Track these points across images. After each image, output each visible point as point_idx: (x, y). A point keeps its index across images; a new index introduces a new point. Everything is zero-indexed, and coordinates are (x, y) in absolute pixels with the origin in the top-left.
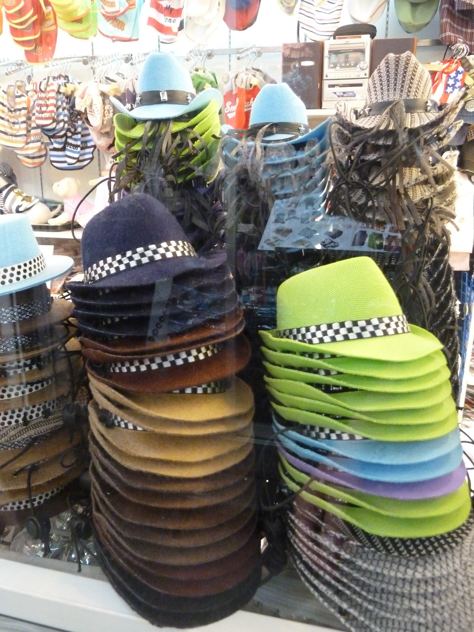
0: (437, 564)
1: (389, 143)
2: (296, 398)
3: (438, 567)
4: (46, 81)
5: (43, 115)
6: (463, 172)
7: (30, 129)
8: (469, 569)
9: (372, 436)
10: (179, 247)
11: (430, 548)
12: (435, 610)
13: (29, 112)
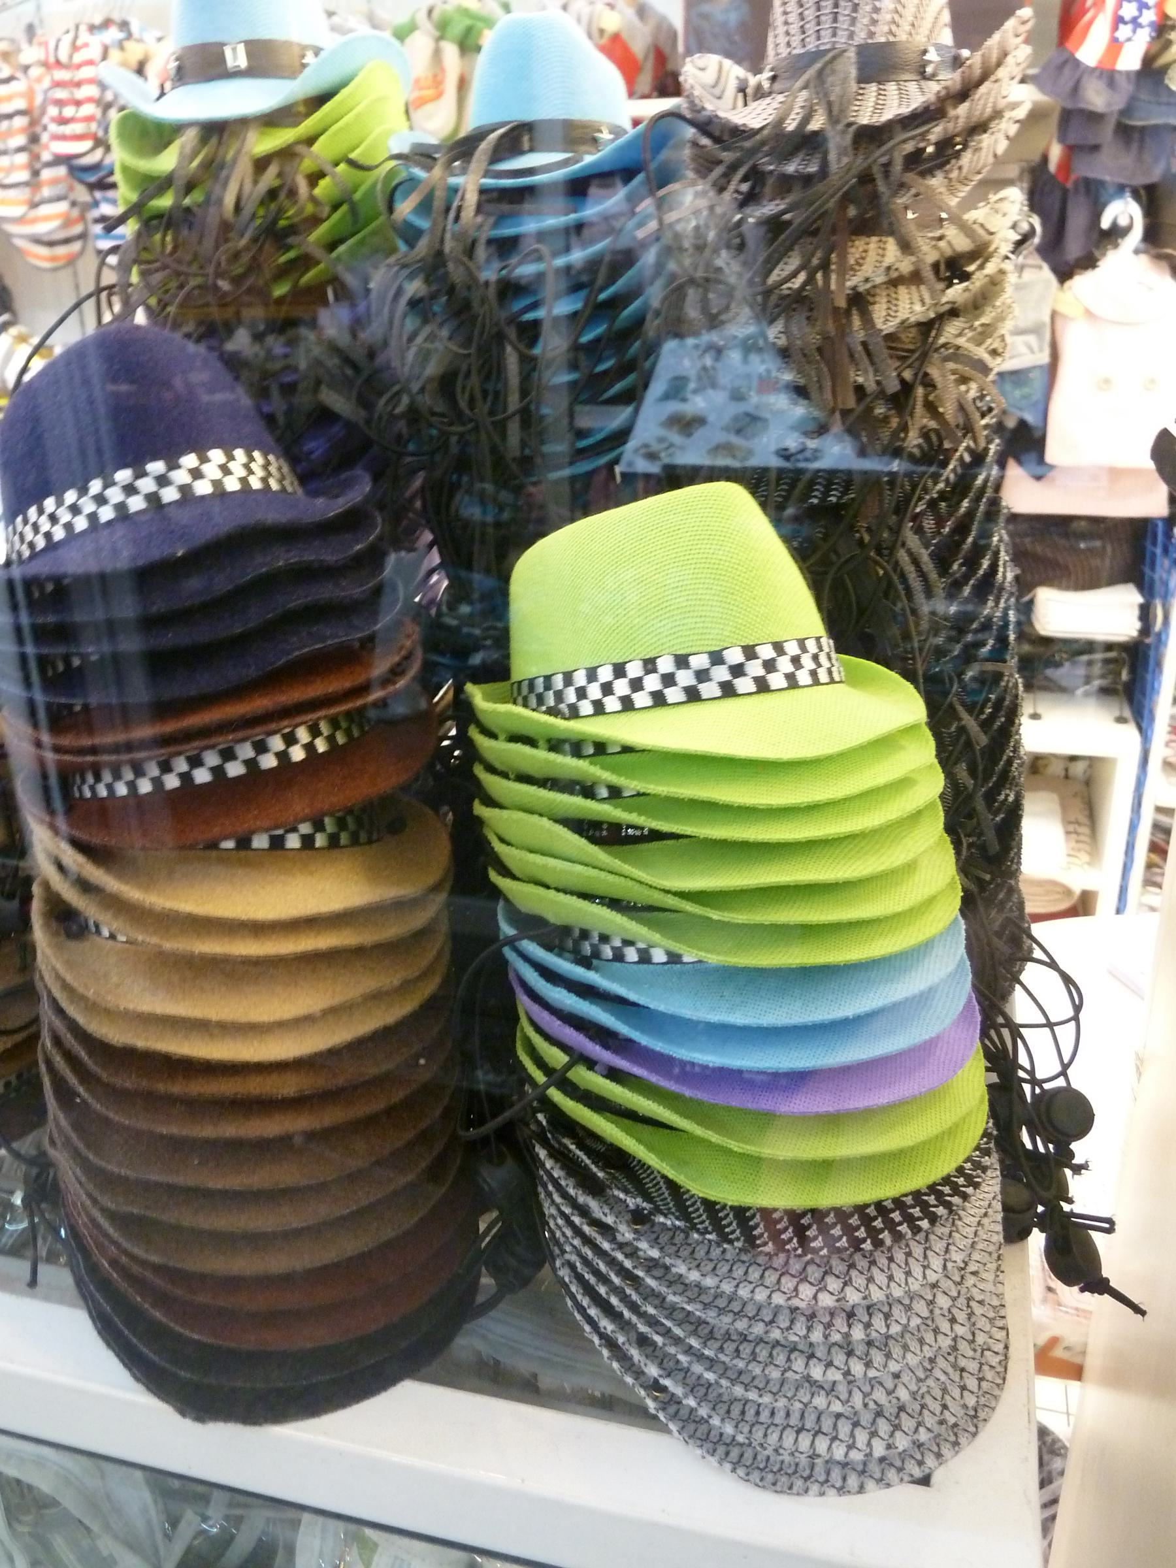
0: (882, 1271)
1: (813, 169)
2: (533, 858)
3: (880, 1278)
4: (71, 35)
5: (68, 129)
6: (1159, 257)
7: (38, 166)
8: (970, 1281)
9: (709, 956)
10: (232, 465)
11: (861, 1233)
12: (875, 1383)
13: (33, 123)
